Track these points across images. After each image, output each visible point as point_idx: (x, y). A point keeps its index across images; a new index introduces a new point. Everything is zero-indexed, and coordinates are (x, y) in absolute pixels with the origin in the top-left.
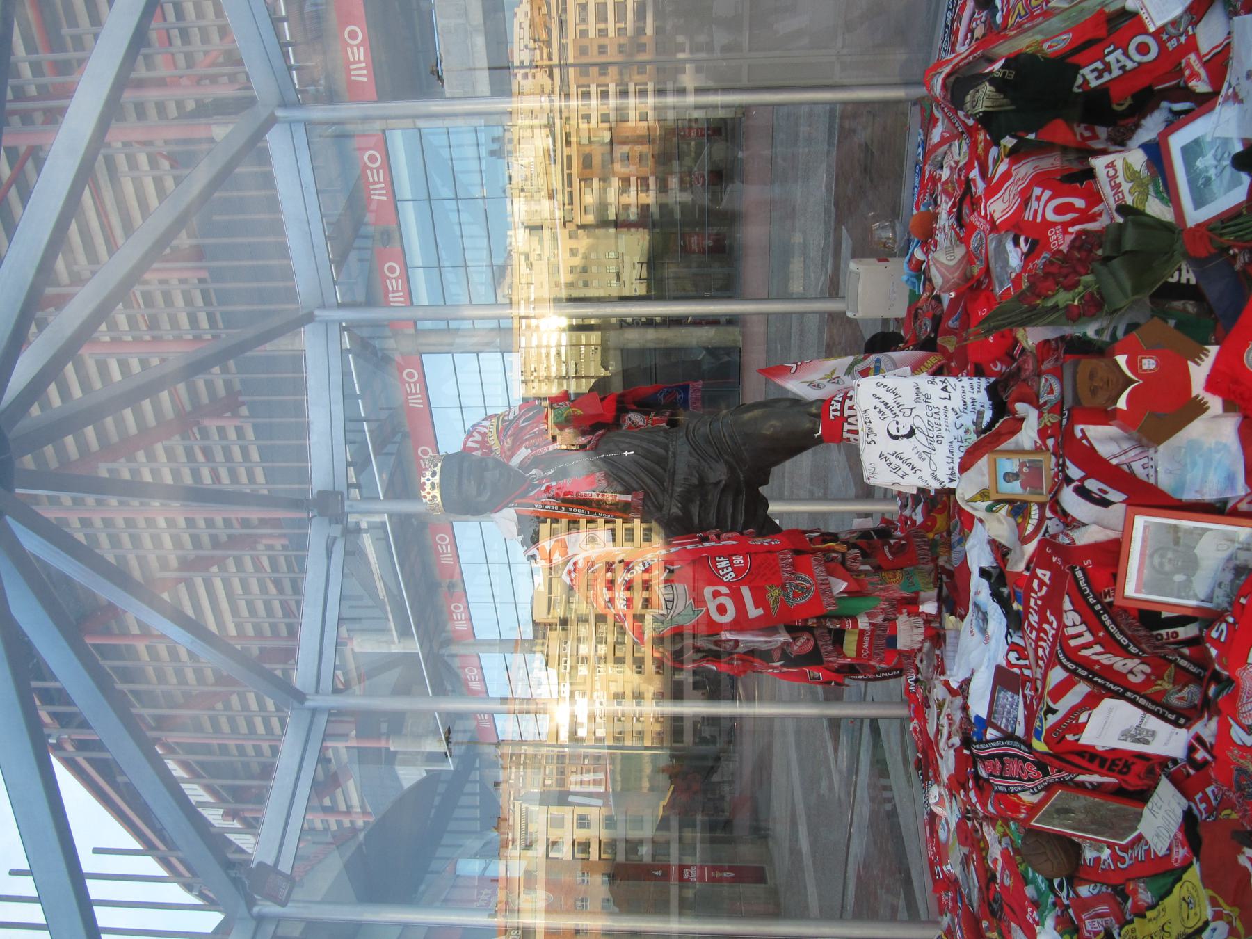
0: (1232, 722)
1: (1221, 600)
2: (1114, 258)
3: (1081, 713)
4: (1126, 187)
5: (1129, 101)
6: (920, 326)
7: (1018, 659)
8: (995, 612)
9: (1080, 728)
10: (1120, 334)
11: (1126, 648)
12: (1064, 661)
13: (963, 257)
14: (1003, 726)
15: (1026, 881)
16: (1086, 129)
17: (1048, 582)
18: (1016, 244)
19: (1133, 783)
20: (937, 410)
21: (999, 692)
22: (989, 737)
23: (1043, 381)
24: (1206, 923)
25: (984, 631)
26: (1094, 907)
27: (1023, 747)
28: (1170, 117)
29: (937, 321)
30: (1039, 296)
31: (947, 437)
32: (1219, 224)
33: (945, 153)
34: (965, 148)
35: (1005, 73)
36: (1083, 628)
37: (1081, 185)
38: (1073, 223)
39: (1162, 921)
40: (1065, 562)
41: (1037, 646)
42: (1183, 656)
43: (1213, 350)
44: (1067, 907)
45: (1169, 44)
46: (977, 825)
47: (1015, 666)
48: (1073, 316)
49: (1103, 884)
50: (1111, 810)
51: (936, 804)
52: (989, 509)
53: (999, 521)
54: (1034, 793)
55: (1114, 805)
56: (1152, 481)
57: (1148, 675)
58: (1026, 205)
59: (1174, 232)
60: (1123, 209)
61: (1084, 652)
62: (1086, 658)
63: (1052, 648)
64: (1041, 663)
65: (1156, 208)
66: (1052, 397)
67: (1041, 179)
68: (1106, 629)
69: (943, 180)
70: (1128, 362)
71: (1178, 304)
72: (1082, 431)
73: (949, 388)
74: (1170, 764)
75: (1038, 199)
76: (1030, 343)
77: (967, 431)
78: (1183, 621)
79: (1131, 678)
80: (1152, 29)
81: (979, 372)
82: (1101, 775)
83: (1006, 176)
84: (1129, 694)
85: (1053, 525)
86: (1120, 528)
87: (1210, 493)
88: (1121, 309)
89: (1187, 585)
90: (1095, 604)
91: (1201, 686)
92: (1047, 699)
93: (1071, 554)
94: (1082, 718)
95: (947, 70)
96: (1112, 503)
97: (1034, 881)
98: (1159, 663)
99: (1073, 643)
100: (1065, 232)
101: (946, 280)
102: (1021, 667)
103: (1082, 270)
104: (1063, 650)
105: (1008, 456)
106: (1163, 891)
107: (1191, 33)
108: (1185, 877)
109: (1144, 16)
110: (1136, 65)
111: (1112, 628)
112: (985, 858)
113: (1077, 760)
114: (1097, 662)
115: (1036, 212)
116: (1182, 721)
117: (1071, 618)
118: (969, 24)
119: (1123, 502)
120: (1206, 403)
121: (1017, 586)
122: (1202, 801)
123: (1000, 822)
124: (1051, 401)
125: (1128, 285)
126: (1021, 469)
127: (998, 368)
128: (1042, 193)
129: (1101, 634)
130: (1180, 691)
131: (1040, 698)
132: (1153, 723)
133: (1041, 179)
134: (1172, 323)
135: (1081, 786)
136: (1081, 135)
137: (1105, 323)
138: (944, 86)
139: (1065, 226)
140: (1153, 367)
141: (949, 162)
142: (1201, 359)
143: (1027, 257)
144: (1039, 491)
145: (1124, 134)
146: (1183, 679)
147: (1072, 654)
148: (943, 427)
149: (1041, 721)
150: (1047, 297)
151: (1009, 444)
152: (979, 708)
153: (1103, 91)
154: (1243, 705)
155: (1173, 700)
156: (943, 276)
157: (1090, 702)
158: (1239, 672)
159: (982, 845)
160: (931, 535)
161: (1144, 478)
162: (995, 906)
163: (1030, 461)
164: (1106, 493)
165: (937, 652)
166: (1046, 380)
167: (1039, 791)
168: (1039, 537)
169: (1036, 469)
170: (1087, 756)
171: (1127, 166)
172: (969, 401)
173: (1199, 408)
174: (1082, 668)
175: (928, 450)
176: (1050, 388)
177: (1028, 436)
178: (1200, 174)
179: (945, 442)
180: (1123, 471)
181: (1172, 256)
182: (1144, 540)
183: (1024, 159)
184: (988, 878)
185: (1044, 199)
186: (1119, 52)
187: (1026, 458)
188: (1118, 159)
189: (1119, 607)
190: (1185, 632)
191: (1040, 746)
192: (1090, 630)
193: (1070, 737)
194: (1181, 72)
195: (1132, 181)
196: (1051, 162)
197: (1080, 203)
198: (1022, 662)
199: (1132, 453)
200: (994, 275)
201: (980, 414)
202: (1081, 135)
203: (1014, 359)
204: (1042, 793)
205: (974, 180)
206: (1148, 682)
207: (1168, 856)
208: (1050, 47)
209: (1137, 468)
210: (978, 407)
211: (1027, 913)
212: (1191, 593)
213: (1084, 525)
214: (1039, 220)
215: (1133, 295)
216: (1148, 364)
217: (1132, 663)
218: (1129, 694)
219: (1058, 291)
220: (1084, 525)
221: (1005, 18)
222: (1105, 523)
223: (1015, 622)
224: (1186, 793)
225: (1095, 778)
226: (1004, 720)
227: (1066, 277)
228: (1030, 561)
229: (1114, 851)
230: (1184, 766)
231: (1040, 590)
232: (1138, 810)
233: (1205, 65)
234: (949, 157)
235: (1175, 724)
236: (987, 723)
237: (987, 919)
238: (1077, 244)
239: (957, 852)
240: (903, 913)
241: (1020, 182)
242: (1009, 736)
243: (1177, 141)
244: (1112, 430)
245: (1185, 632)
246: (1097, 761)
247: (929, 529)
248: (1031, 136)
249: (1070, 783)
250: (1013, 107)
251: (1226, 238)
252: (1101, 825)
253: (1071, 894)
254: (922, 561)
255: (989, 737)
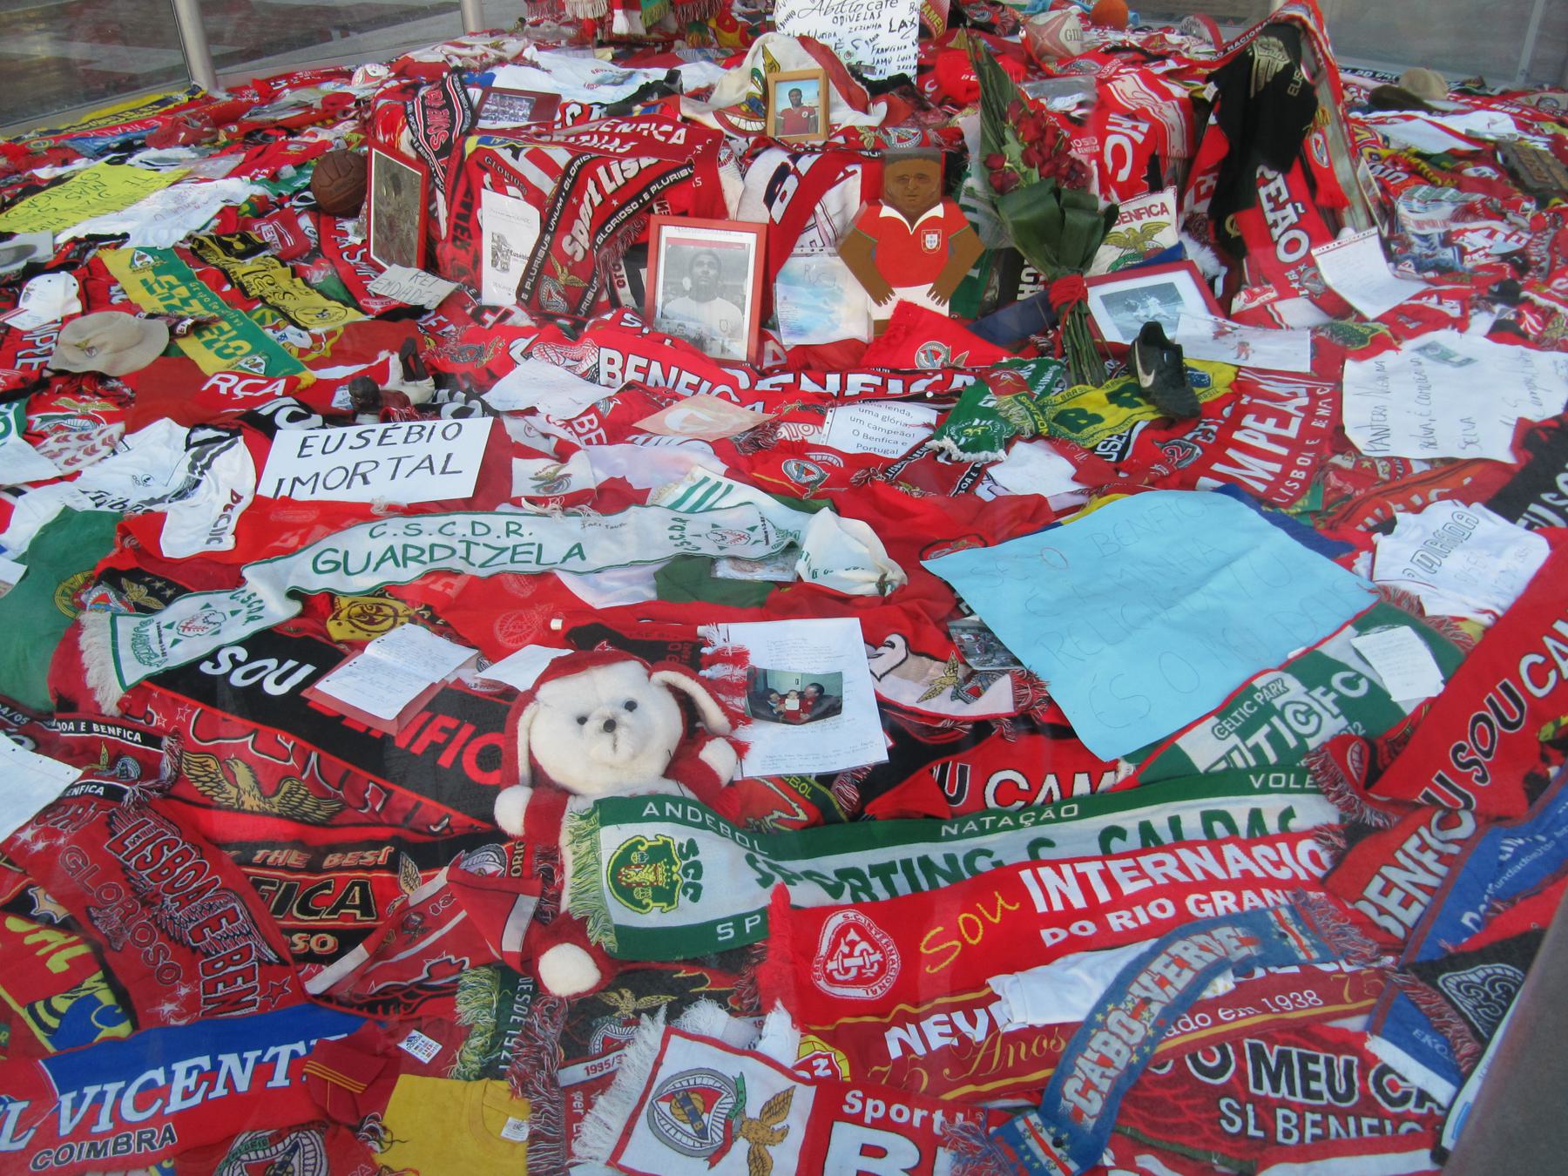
0: (532, 338)
1: (664, 327)
2: (1058, 201)
3: (518, 187)
4: (1137, 225)
5: (1233, 233)
6: (982, 8)
7: (572, 115)
8: (631, 89)
9: (499, 187)
10: (968, 215)
11: (601, 229)
12: (578, 163)
13: (1067, 51)
14: (487, 106)
15: (299, 165)
16: (1210, 188)
17: (670, 142)
18: (1080, 105)
19: (445, 251)
20: (876, 15)
21: (527, 100)
22: (471, 91)
23: (914, 131)
24: (305, 329)
25: (601, 83)
26: (290, 232)
27: (466, 127)
28: (1209, 277)
29: (987, 29)
30: (1017, 123)
31: (843, 30)
32: (1084, 311)
33: (1200, 38)
34: (1202, 58)
35: (1297, 83)
36: (620, 181)
37: (1145, 178)
38: (1102, 166)
39: (294, 292)
40: (697, 157)
41: (592, 134)
42: (597, 295)
43: (944, 310)
44: (282, 207)
45: (1293, 272)
46: (352, 114)
47: (564, 114)
48: (992, 163)
49: (319, 240)
50: (408, 234)
51: (366, 72)
52: (755, 72)
53: (741, 87)
54: (412, 144)
55: (415, 237)
56: (797, 250)
57: (572, 257)
58: (1128, 117)
59: (1081, 266)
60: (1112, 215)
61: (591, 185)
62: (585, 187)
63: (593, 149)
64: (572, 140)
65: (1106, 256)
66: (894, 140)
67: (1158, 132)
68: (622, 207)
69: (1167, 35)
70: (934, 218)
71: (996, 281)
72: (854, 172)
73: (904, 30)
74: (473, 291)
75: (1135, 128)
76: (960, 120)
77: (849, 54)
78: (638, 291)
79: (567, 239)
80: (1314, 252)
81: (922, 69)
82: (448, 219)
83: (1166, 95)
84: (548, 238)
85: (740, 144)
86: (741, 218)
87: (782, 310)
88: (997, 212)
89: (675, 290)
90: (650, 193)
91: (568, 312)
92: (529, 147)
93: (708, 164)
94: (511, 190)
95: (1312, 24)
96: (770, 208)
97: (300, 175)
98: (586, 269)
99: (601, 171)
100: (1092, 156)
101: (1040, 29)
102: (563, 120)
103: (1047, 168)
104: (587, 165)
105: (822, 94)
106: (328, 291)
107: (1301, 293)
108: (351, 310)
109: (1331, 245)
110: (1276, 238)
111: (623, 215)
112: (313, 124)
113: (461, 189)
114: (581, 201)
115: (1119, 125)
116: (524, 296)
117: (631, 167)
118: (1354, 85)
119: (771, 219)
120: (886, 303)
121: (662, 108)
122: (439, 322)
123: (362, 137)
124: (890, 140)
125: (1025, 217)
126: (805, 108)
127: (927, 89)
128: (1141, 133)
129: (615, 202)
130: (558, 293)
131: (529, 140)
132: (518, 268)
133: (1158, 132)
134: (975, 273)
135: (430, 198)
136: (1203, 182)
137: (980, 195)
138: (1293, 18)
139: (1099, 156)
140: (935, 237)
141: (1188, 42)
142: (935, 297)
143: (1065, 116)
144: (780, 130)
145: (1197, 230)
146: (574, 297)
147: (587, 171)
148: (854, 24)
149: (501, 143)
150: (1015, 132)
151: (836, 96)
152: (505, 78)
153: (1254, 202)
154: (552, 348)
155: (547, 286)
156: (1047, 25)
157: (533, 195)
158: (588, 340)
159: (329, 122)
160: (712, 23)
161: (799, 243)
162: (259, 137)
163: (816, 120)
164: (782, 200)
165: (563, 43)
166: (915, 135)
167: (416, 149)
168: (726, 132)
169: (807, 126)
170: (468, 200)
171: (1160, 227)
172: (887, 55)
173: (880, 296)
174: (573, 183)
175: (824, 6)
176: (905, 139)
177: (845, 116)
178: (1141, 301)
179: (836, 28)
180: (807, 219)
181: (1053, 264)
182: (728, 245)
183: (1185, 115)
184: (292, 129)
185: (1136, 135)
186: (1295, 219)
187: (820, 114)
188: (1171, 217)
189: (648, 221)
190: (625, 294)
191: (471, 144)
192: (619, 188)
193: (487, 178)
194: (1259, 285)
195: (1142, 232)
196: (1176, 144)
197: (1123, 175)
198: (569, 121)
199: (828, 229)
200: (1046, 82)
201: (872, 69)
202: (1203, 182)
203: (940, 105)
204: (413, 155)
205: (1164, 64)
206: (565, 259)
207: (368, 295)
208: (1317, 142)
209: (812, 234)
210: (879, 67)
211: (260, 168)
212: (671, 296)
213: (743, 177)
214: (1108, 128)
215: (1013, 223)
216: (932, 241)
217: (584, 239)
218: (548, 238)
219: (1022, 144)
220: (743, 177)
221: (1356, 120)
222: (745, 200)
223: (619, 111)
224: (441, 308)
225: (442, 213)
226: (494, 108)
227: (1040, 152)
228: (694, 122)
229: (360, 247)
230: (473, 304)
231: (661, 133)
232: (415, 263)
233: (1263, 307)
234: (1196, 42)
235: (520, 290)
236: (488, 89)
237: (240, 129)
238: (1077, 167)
239: (314, 96)
240: (217, 50)
241: (1157, 110)
242: (476, 114)
243: (1181, 280)
244: (855, 205)
245: (625, 294)
246: (462, 211)
247: (720, 22)
248: (1212, 120)
249: (432, 185)
250: (1252, 95)
251: (1069, 318)
252: (389, 227)
253: (299, 210)
254: (679, 11)
255: (471, 91)
